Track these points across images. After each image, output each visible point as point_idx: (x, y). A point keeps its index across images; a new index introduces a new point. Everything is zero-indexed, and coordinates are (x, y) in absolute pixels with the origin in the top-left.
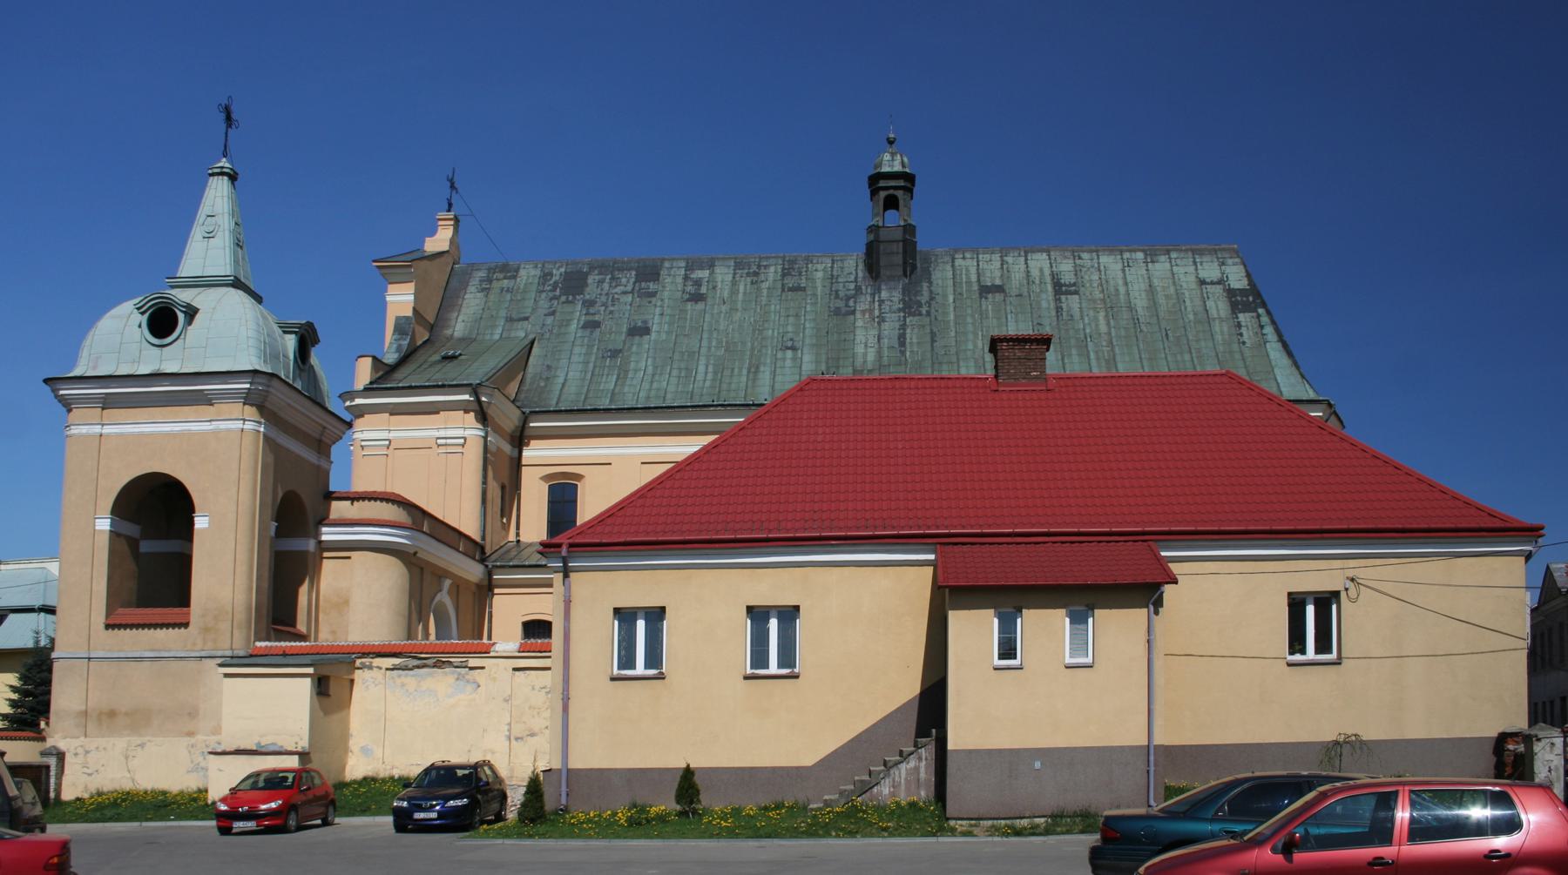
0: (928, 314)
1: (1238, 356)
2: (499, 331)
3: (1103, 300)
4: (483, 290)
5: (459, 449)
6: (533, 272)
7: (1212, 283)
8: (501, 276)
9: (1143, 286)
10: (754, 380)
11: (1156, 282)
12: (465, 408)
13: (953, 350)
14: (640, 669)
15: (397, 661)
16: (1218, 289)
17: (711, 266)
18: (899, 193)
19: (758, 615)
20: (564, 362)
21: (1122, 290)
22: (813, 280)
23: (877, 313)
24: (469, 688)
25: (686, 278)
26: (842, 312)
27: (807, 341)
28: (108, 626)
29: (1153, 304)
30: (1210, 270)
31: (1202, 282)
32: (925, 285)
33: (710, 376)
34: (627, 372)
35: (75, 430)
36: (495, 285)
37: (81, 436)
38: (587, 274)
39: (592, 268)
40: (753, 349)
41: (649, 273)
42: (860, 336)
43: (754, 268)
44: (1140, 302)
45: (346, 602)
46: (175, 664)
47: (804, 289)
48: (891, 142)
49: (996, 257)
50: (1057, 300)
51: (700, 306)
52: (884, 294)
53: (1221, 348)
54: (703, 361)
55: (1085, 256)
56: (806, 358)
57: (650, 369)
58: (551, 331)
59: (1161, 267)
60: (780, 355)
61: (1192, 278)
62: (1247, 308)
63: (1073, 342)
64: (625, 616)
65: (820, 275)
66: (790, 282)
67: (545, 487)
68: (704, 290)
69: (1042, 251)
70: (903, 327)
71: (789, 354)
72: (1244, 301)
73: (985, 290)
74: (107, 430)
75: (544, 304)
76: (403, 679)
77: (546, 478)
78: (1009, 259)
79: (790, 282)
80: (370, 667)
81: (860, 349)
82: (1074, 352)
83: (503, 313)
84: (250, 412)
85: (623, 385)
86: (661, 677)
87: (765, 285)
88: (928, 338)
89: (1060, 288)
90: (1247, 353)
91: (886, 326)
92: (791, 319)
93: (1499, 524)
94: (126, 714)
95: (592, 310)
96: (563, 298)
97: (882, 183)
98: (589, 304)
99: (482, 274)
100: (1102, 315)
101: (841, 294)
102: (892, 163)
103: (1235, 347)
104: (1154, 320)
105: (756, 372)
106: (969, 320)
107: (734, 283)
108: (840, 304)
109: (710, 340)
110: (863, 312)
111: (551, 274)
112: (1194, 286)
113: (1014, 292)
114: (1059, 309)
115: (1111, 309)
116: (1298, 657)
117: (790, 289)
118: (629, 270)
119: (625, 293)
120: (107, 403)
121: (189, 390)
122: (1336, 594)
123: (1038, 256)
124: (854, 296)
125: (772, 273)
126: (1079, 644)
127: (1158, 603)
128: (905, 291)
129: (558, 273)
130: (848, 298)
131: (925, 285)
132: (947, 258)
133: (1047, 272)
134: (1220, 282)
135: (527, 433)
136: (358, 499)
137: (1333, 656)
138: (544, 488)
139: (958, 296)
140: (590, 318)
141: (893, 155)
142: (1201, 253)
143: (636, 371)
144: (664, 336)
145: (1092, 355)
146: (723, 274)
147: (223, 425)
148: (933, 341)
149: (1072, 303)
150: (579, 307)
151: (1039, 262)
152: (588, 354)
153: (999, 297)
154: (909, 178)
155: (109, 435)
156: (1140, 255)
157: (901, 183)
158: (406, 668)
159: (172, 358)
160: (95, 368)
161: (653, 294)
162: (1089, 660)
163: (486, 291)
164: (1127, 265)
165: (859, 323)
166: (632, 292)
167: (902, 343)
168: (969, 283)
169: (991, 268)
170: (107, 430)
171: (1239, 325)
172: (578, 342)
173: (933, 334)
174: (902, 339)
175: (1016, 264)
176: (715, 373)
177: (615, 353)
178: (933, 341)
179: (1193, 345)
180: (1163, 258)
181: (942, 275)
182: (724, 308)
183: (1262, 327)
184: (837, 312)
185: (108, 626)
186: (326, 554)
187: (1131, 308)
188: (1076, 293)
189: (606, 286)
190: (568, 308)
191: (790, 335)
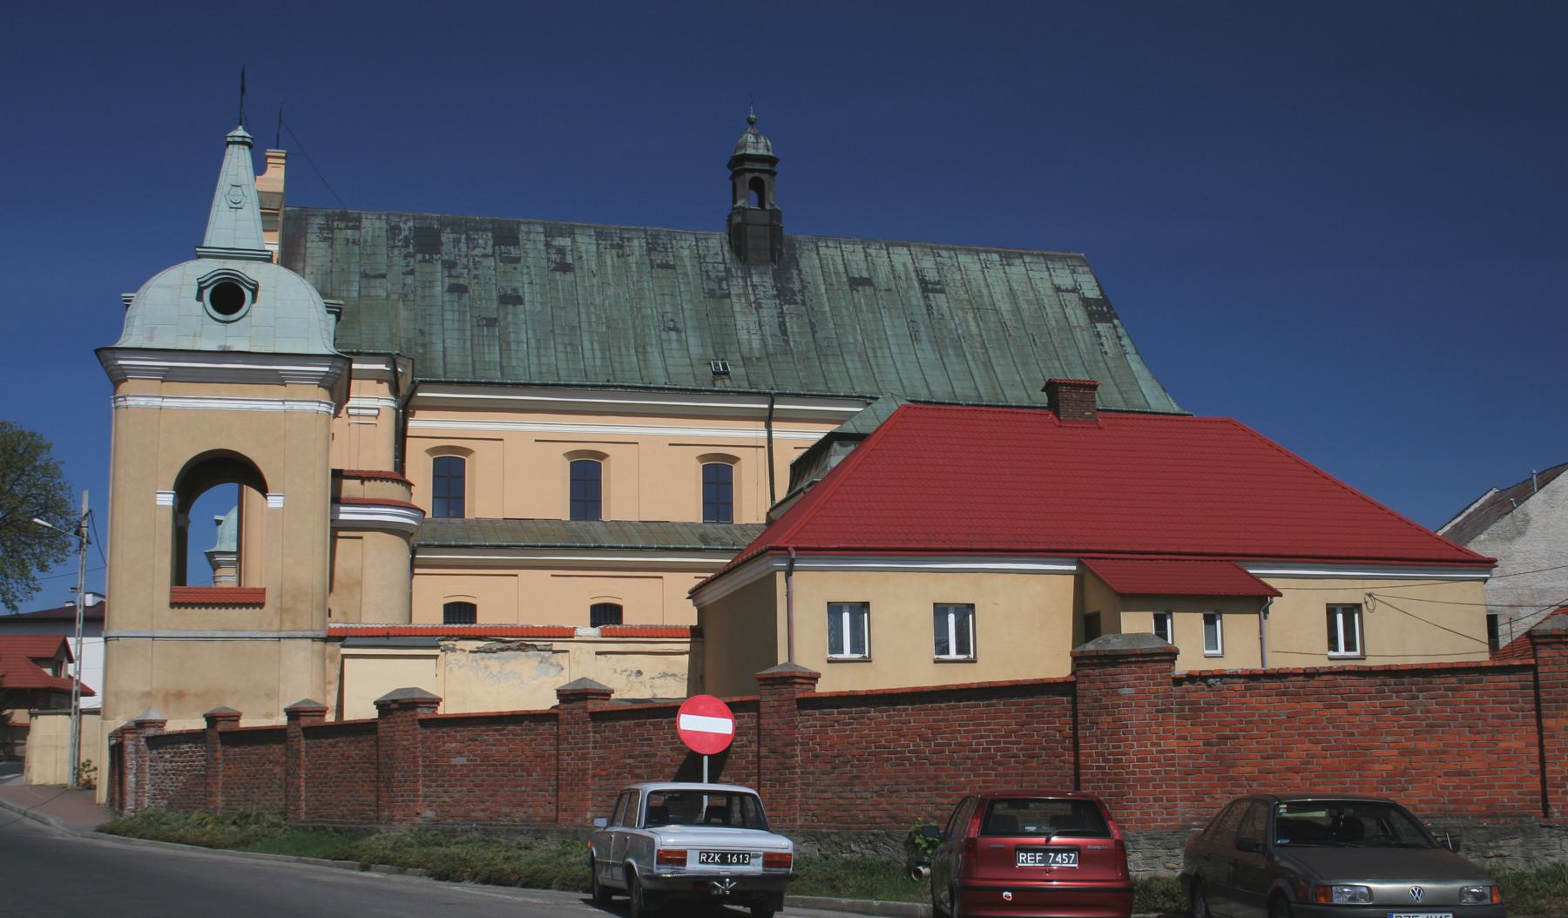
0: (804, 303)
1: (1102, 365)
2: (356, 287)
3: (970, 302)
4: (325, 239)
5: (373, 421)
6: (377, 224)
7: (1067, 291)
8: (342, 225)
9: (1005, 289)
10: (645, 361)
11: (1015, 286)
12: (378, 377)
13: (835, 343)
14: (847, 653)
15: (481, 644)
16: (1073, 297)
17: (572, 234)
18: (764, 177)
19: (940, 610)
20: (437, 328)
21: (985, 292)
22: (681, 259)
23: (752, 298)
24: (553, 670)
25: (548, 245)
26: (718, 295)
27: (689, 323)
28: (173, 605)
29: (1017, 310)
30: (1064, 278)
31: (1058, 289)
32: (795, 272)
33: (598, 354)
34: (508, 344)
35: (131, 402)
36: (337, 234)
37: (138, 407)
38: (439, 232)
39: (443, 225)
40: (635, 328)
41: (507, 237)
42: (740, 320)
43: (617, 240)
44: (1005, 306)
45: (359, 583)
46: (249, 645)
47: (673, 267)
48: (751, 123)
49: (859, 248)
50: (926, 298)
51: (569, 277)
52: (756, 279)
53: (1086, 357)
54: (586, 338)
55: (944, 253)
56: (692, 341)
57: (532, 342)
58: (414, 292)
59: (1017, 270)
60: (664, 336)
61: (1048, 285)
62: (1105, 318)
63: (948, 342)
64: (835, 609)
65: (686, 253)
66: (658, 258)
67: (430, 461)
68: (569, 260)
69: (902, 245)
70: (781, 314)
71: (673, 335)
72: (1098, 311)
73: (856, 283)
74: (167, 403)
75: (399, 262)
76: (486, 662)
77: (432, 451)
78: (871, 251)
79: (658, 258)
80: (454, 650)
81: (743, 336)
82: (951, 351)
83: (355, 268)
84: (323, 394)
85: (510, 358)
86: (868, 660)
87: (632, 260)
88: (808, 329)
89: (926, 287)
90: (1111, 364)
91: (764, 312)
92: (667, 299)
93: (1465, 557)
94: (197, 695)
95: (454, 272)
96: (419, 257)
97: (748, 165)
98: (450, 265)
99: (320, 221)
100: (970, 316)
101: (713, 275)
102: (755, 145)
103: (1099, 356)
104: (1020, 325)
105: (644, 353)
106: (845, 312)
107: (599, 255)
108: (714, 286)
109: (588, 314)
110: (739, 296)
111: (399, 228)
112: (1051, 292)
113: (883, 286)
114: (929, 307)
115: (978, 310)
116: (1332, 654)
117: (660, 266)
118: (485, 230)
119: (486, 256)
120: (168, 376)
121: (263, 369)
122: (1358, 607)
123: (898, 250)
124: (726, 279)
125: (637, 246)
126: (1211, 641)
127: (1266, 611)
128: (776, 277)
129: (407, 227)
130: (720, 280)
131: (795, 272)
132: (812, 246)
133: (911, 268)
134: (1074, 290)
135: (413, 402)
136: (369, 479)
137: (1357, 653)
138: (429, 462)
139: (829, 286)
140: (455, 281)
141: (757, 136)
142: (1052, 259)
143: (519, 343)
144: (539, 308)
145: (969, 357)
146: (586, 244)
147: (297, 406)
148: (814, 332)
149: (940, 301)
150: (439, 267)
151: (901, 256)
152: (462, 321)
153: (869, 290)
154: (772, 161)
155: (168, 408)
156: (995, 257)
157: (767, 167)
158: (490, 651)
159: (240, 335)
160: (151, 339)
161: (517, 260)
162: (1219, 651)
163: (330, 241)
164: (985, 267)
165: (737, 308)
166: (493, 255)
167: (784, 332)
168: (837, 273)
169: (854, 257)
170: (167, 403)
171: (1099, 335)
172: (447, 306)
173: (812, 325)
174: (782, 325)
175: (880, 256)
176: (602, 351)
177: (491, 322)
178: (814, 332)
179: (1060, 351)
180: (1018, 262)
181: (809, 262)
182: (595, 281)
183: (1120, 338)
184: (711, 294)
185: (173, 605)
186: (341, 534)
187: (996, 311)
188: (942, 291)
189: (463, 246)
190: (428, 268)
191: (670, 316)
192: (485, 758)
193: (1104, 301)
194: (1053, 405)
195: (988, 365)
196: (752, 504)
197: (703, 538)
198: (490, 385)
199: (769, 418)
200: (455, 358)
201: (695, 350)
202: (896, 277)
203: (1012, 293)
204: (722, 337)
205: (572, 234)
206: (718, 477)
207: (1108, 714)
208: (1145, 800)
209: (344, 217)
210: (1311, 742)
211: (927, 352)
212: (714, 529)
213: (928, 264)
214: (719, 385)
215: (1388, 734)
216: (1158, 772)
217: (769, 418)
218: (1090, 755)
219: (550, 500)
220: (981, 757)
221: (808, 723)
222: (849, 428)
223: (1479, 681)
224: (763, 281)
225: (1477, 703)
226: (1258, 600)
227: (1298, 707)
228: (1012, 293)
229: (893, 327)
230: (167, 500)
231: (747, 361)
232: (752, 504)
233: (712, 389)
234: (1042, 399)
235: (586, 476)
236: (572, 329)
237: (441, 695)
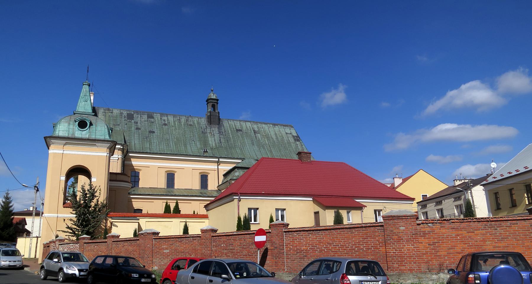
18: (216, 104)
25: (161, 119)
29: (277, 138)
38: (133, 115)
42: (210, 139)
44: (274, 137)
51: (166, 127)
54: (171, 142)
62: (298, 141)
68: (166, 122)
81: (210, 143)
107: (174, 122)
114: (256, 137)
128: (218, 128)
139: (231, 131)
149: (259, 135)
152: (139, 137)
153: (241, 132)
185: (64, 207)
187: (272, 138)
192: (176, 250)
193: (298, 136)
194: (300, 158)
195: (271, 151)
196: (213, 185)
197: (201, 193)
198: (147, 153)
199: (218, 163)
200: (137, 146)
201: (199, 146)
202: (248, 130)
203: (276, 134)
204: (205, 143)
205: (167, 115)
206: (204, 179)
207: (396, 235)
208: (410, 263)
209: (109, 110)
210: (464, 244)
211: (256, 148)
212: (204, 191)
213: (255, 127)
214: (205, 155)
215: (489, 241)
216: (414, 254)
217: (218, 163)
218: (390, 248)
219: (162, 183)
220: (350, 249)
221: (286, 239)
222: (239, 165)
223: (517, 224)
224: (215, 130)
225: (516, 231)
226: (360, 207)
227: (460, 232)
228: (276, 134)
229: (247, 141)
230: (63, 178)
231: (212, 149)
232: (213, 185)
233: (204, 154)
234: (296, 157)
235: (170, 177)
236: (168, 140)
237: (217, 228)
